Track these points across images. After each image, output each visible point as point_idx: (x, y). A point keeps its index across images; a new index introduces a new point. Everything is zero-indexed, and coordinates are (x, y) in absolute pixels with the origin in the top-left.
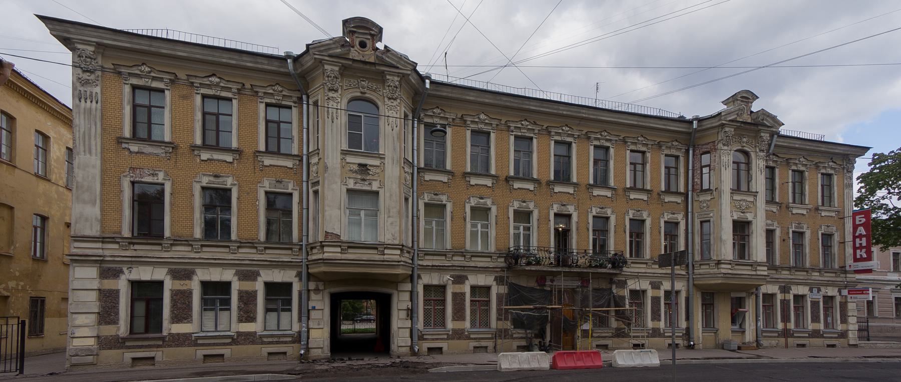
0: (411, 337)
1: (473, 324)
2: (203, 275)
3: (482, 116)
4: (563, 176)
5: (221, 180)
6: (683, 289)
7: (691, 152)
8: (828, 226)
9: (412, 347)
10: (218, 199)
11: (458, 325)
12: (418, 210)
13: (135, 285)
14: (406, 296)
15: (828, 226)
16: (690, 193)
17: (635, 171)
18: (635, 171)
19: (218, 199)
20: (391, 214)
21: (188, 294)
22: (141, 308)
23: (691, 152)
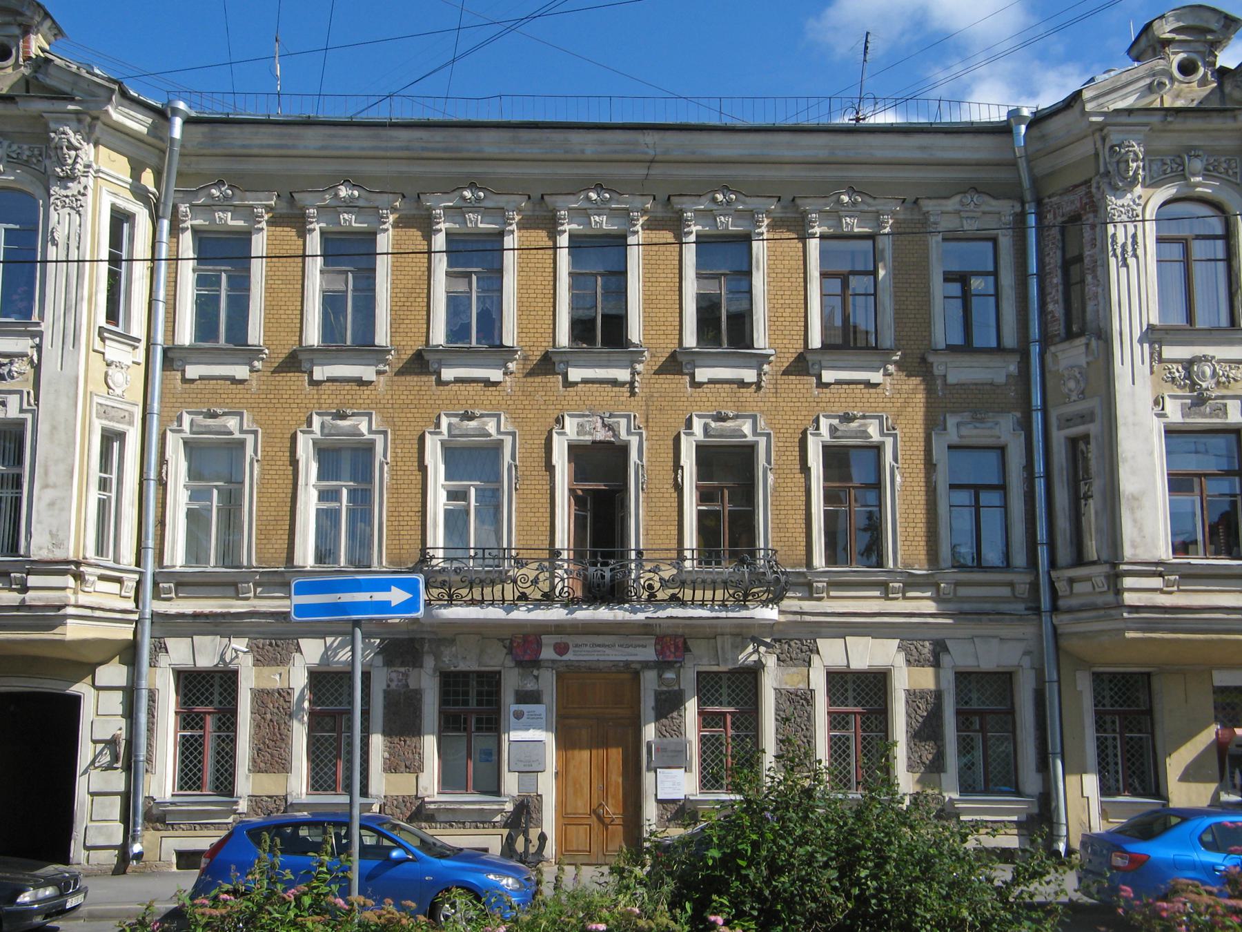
0: (125, 819)
1: (448, 781)
2: (831, 653)
3: (343, 192)
4: (602, 330)
5: (729, 424)
6: (1026, 662)
7: (1032, 220)
8: (847, 418)
9: (124, 849)
10: (729, 467)
11: (269, 785)
12: (162, 461)
13: (838, 680)
14: (115, 702)
15: (847, 418)
16: (1035, 349)
17: (966, 297)
18: (966, 297)
19: (729, 467)
20: (52, 479)
21: (804, 699)
22: (853, 733)
23: (1032, 220)
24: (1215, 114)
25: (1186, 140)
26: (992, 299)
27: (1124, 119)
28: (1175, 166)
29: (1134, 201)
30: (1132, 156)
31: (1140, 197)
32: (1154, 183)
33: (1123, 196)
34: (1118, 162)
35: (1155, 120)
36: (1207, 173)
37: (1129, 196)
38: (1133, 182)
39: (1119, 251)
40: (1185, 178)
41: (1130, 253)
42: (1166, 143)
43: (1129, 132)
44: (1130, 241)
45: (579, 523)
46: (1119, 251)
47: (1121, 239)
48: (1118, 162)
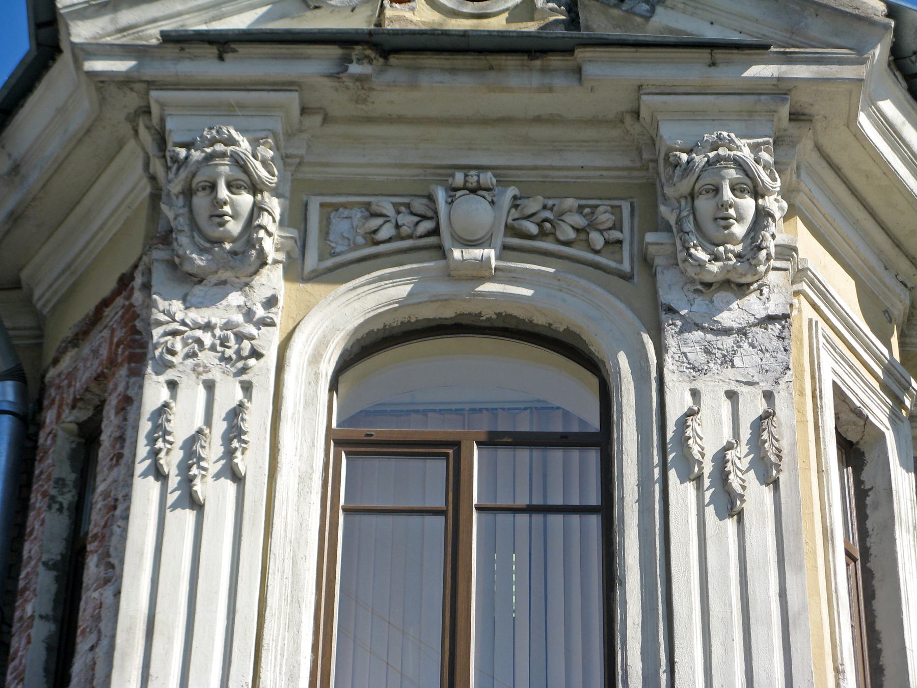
24: (511, 61)
25: (444, 148)
26: (594, 521)
27: (207, 67)
28: (407, 220)
29: (249, 314)
30: (225, 168)
31: (271, 302)
32: (317, 266)
33: (211, 302)
34: (188, 193)
35: (313, 66)
36: (517, 240)
37: (235, 298)
38: (244, 258)
39: (171, 462)
40: (441, 252)
41: (214, 467)
42: (376, 158)
43: (229, 112)
44: (220, 426)
45: (726, 531)
46: (171, 462)
47: (181, 426)
48: (188, 193)
